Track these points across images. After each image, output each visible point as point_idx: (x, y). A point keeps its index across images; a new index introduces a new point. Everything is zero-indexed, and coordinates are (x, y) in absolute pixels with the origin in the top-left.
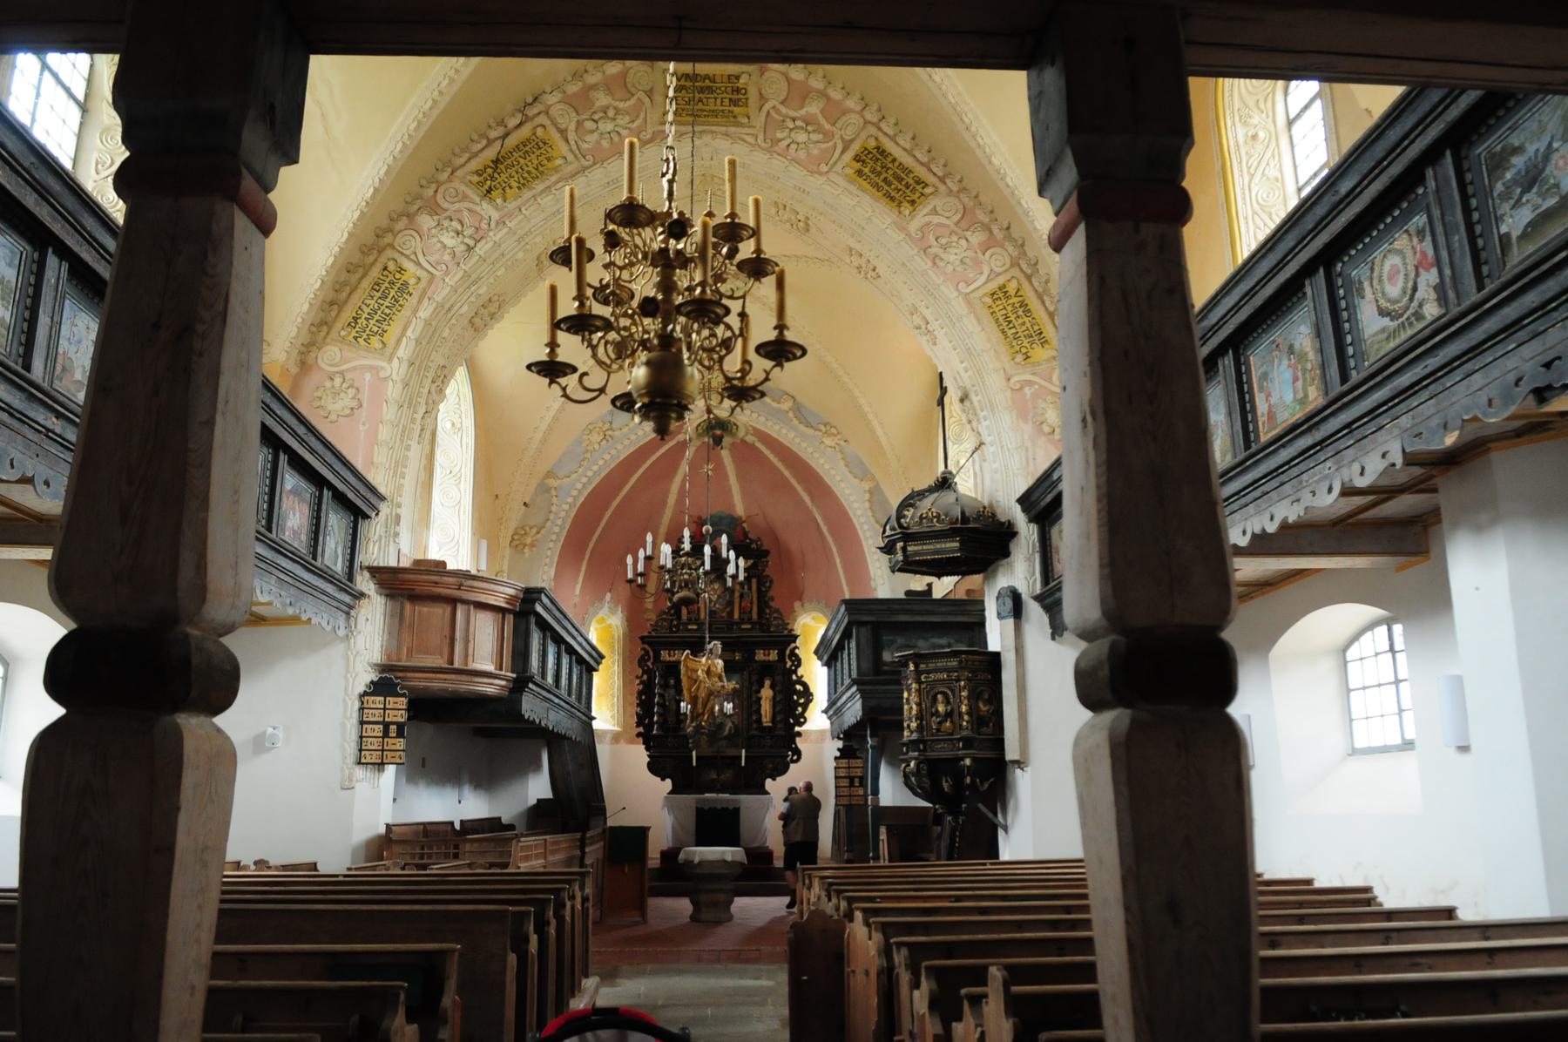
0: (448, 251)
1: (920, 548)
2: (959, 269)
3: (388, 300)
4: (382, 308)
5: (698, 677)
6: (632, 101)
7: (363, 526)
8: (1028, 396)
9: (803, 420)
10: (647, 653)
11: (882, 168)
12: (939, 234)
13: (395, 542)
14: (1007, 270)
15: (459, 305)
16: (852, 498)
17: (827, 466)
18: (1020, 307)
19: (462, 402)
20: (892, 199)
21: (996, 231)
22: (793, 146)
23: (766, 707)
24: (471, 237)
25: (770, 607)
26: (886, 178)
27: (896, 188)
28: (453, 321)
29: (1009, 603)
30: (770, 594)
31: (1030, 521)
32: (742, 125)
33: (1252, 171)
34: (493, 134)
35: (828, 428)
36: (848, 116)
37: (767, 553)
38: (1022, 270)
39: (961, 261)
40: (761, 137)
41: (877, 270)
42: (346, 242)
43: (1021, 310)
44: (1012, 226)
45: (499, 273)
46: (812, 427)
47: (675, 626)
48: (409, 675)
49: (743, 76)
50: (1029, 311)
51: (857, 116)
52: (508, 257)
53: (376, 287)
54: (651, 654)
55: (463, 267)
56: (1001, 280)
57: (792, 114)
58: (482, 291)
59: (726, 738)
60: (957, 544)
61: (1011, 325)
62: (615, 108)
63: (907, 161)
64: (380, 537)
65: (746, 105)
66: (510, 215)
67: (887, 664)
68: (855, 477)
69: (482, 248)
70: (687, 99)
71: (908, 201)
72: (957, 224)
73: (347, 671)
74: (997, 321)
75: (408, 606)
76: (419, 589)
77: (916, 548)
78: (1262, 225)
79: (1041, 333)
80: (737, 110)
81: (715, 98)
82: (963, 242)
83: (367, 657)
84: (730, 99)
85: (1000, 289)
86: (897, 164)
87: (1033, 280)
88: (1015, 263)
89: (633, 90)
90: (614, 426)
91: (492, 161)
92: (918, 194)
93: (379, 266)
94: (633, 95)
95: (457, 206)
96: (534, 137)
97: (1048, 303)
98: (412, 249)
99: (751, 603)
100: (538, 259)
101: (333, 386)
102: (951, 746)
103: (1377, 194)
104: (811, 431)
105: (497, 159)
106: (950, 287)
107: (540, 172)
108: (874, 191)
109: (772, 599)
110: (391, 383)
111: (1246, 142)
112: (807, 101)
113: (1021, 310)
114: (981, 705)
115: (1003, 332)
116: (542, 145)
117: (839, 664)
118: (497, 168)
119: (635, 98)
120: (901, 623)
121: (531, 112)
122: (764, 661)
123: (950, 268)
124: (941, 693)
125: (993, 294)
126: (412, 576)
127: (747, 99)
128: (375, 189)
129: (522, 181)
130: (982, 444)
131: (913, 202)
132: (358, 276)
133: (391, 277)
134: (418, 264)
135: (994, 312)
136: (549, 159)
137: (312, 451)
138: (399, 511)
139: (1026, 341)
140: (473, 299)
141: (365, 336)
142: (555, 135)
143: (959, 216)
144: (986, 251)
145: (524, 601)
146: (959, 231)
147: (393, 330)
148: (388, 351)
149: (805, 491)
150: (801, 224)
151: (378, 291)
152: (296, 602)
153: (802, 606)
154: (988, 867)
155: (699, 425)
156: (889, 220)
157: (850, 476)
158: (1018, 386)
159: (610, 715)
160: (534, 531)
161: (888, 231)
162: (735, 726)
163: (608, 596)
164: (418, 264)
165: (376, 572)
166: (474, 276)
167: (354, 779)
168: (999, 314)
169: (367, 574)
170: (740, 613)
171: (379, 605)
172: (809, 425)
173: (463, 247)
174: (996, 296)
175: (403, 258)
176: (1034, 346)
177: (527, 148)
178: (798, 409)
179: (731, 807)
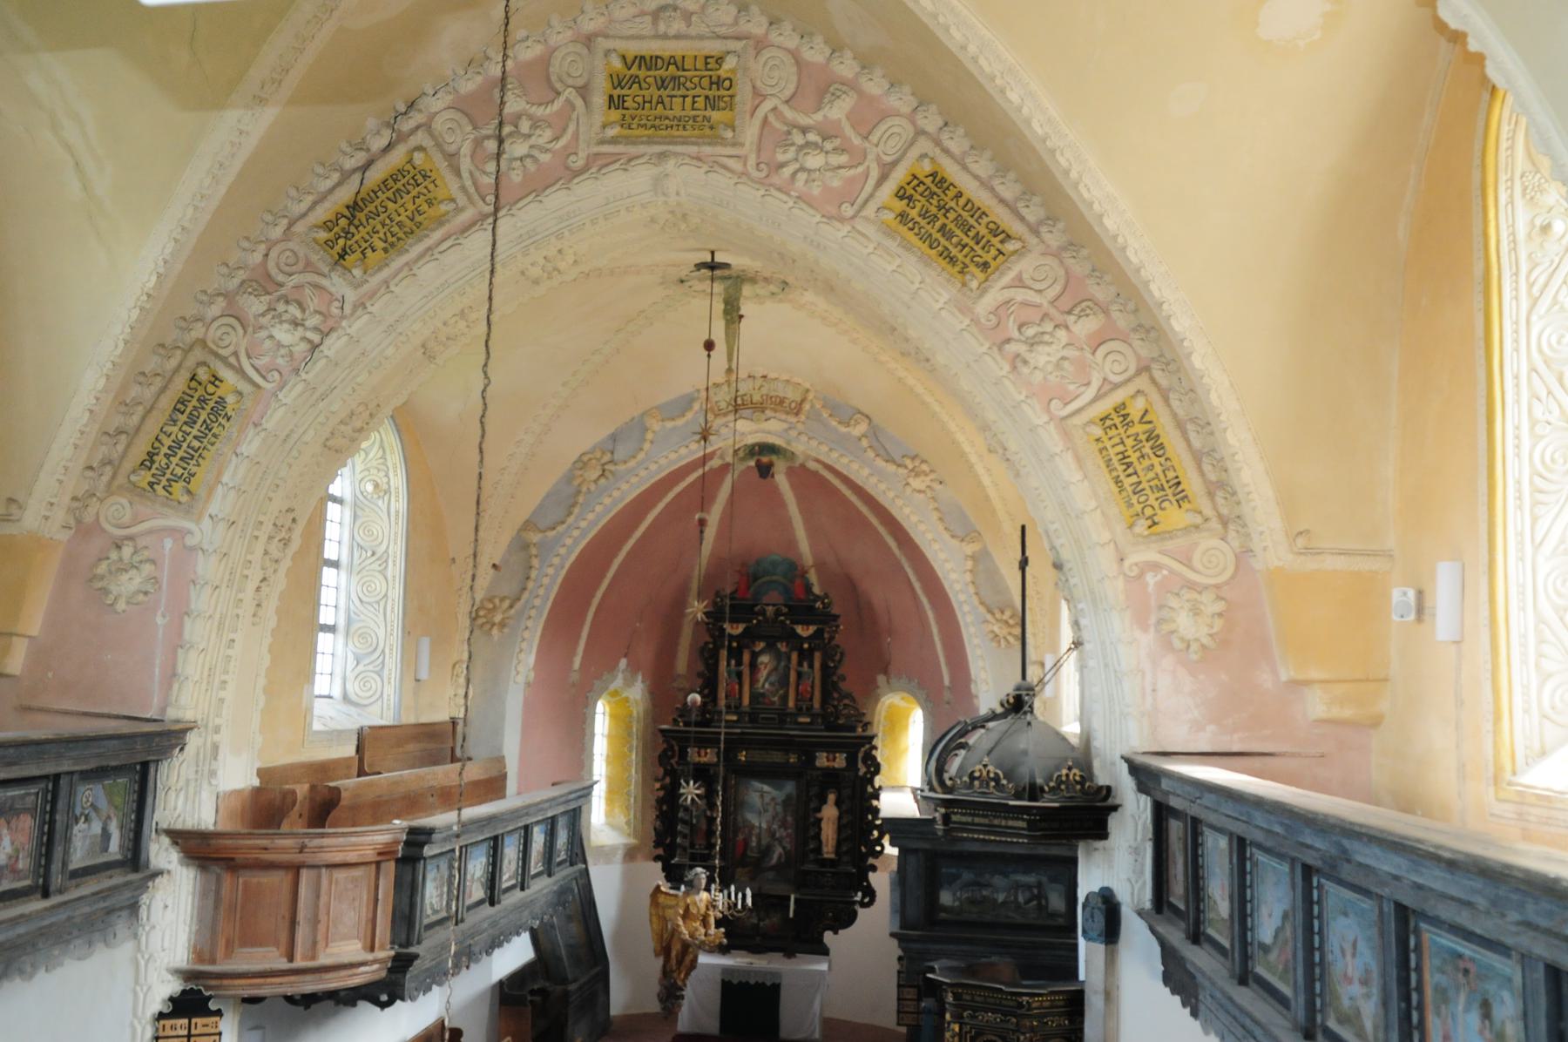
1: (969, 819)
3: (197, 426)
5: (692, 886)
6: (557, 105)
8: (1151, 589)
9: (882, 452)
10: (671, 748)
11: (940, 208)
13: (210, 783)
14: (1129, 380)
18: (1147, 440)
19: (388, 457)
20: (952, 260)
22: (802, 176)
23: (829, 833)
24: (316, 329)
26: (944, 226)
27: (959, 243)
28: (295, 453)
32: (722, 142)
33: (1536, 290)
34: (349, 164)
35: (917, 463)
36: (889, 122)
38: (1153, 381)
40: (752, 161)
42: (120, 356)
45: (359, 380)
46: (894, 462)
48: (226, 982)
49: (728, 58)
50: (1161, 446)
51: (904, 122)
53: (179, 406)
54: (676, 748)
56: (1118, 397)
57: (804, 120)
58: (334, 408)
59: (772, 868)
60: (1023, 824)
62: (530, 117)
63: (982, 198)
64: (188, 781)
65: (731, 107)
66: (372, 295)
67: (945, 909)
68: (953, 536)
69: (333, 346)
70: (639, 99)
71: (977, 265)
72: (1052, 303)
73: (137, 982)
74: (1108, 462)
75: (227, 879)
78: (1543, 394)
79: (1179, 483)
80: (715, 116)
81: (684, 97)
83: (166, 961)
84: (707, 97)
85: (1116, 410)
86: (962, 201)
89: (558, 86)
91: (348, 207)
92: (993, 252)
93: (185, 375)
94: (558, 94)
95: (296, 279)
96: (408, 167)
97: (1192, 436)
98: (231, 349)
99: (812, 687)
101: (121, 559)
104: (891, 468)
105: (355, 203)
107: (415, 227)
108: (925, 247)
109: (843, 678)
110: (200, 552)
111: (1529, 237)
112: (828, 97)
115: (1117, 481)
116: (420, 180)
118: (354, 217)
119: (562, 98)
121: (406, 125)
122: (828, 768)
126: (230, 842)
127: (731, 96)
128: (159, 276)
129: (390, 239)
131: (985, 266)
132: (154, 389)
133: (201, 391)
134: (240, 371)
135: (1105, 448)
136: (430, 203)
138: (216, 738)
139: (1152, 497)
140: (321, 419)
141: (164, 482)
142: (441, 164)
143: (1058, 288)
151: (182, 413)
156: (945, 296)
157: (946, 536)
158: (1135, 572)
159: (625, 820)
160: (507, 603)
161: (943, 313)
162: (787, 853)
163: (623, 663)
164: (240, 371)
165: (180, 837)
168: (1112, 452)
169: (166, 840)
170: (797, 700)
172: (890, 460)
173: (304, 346)
174: (1108, 423)
176: (1166, 504)
177: (399, 185)
178: (875, 433)
179: (768, 983)
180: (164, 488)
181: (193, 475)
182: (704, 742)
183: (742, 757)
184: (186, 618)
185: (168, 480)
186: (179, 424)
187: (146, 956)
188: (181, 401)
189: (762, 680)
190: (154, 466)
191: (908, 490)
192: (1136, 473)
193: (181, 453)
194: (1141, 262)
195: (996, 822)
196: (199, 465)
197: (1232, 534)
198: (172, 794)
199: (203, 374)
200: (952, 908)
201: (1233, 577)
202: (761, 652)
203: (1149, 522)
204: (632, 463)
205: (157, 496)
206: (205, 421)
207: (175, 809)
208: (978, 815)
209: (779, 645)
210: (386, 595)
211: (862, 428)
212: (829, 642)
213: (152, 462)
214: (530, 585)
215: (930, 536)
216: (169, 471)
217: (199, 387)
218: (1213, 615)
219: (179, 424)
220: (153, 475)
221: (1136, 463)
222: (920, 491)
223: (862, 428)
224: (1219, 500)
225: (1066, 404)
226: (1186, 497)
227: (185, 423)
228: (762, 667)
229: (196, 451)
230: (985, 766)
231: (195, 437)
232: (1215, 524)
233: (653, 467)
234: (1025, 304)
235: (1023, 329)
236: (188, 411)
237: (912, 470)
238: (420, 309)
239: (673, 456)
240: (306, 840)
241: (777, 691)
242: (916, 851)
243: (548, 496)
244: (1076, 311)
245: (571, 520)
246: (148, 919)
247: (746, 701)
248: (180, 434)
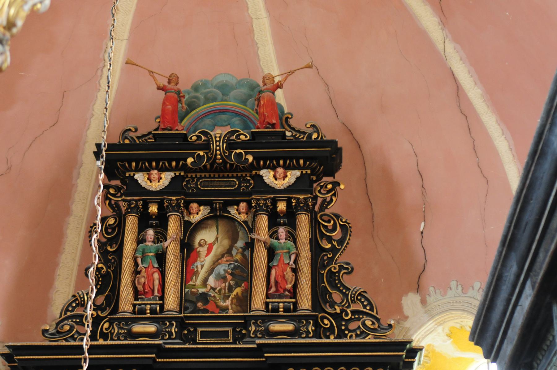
25: (344, 290)
30: (341, 258)
103: (520, 331)
117: (178, 341)
153: (424, 302)
202: (201, 225)
209: (233, 211)
212: (322, 209)
228: (203, 250)
241: (231, 289)
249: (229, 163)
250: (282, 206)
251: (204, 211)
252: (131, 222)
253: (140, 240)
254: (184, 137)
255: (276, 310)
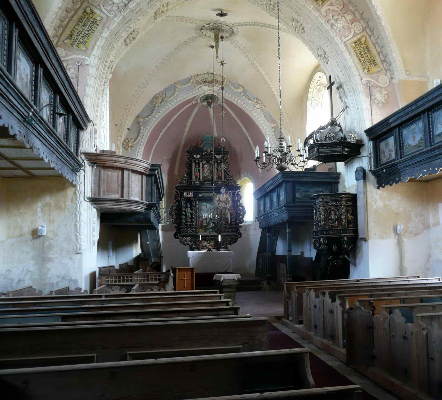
0: (116, 5)
1: (325, 150)
2: (342, 30)
3: (87, 27)
4: (84, 31)
7: (81, 133)
10: (178, 193)
12: (333, 14)
15: (121, 32)
16: (267, 130)
17: (257, 117)
18: (366, 49)
21: (357, 15)
28: (118, 39)
29: (361, 174)
31: (370, 140)
37: (188, 152)
38: (367, 33)
39: (343, 27)
41: (304, 29)
43: (366, 50)
44: (364, 13)
46: (251, 100)
47: (189, 183)
50: (370, 51)
52: (143, 10)
53: (80, 20)
54: (179, 194)
55: (123, 13)
56: (359, 37)
59: (211, 228)
61: (362, 57)
64: (88, 139)
67: (297, 198)
72: (341, 10)
74: (357, 54)
75: (102, 171)
76: (108, 164)
77: (323, 150)
79: (374, 60)
82: (343, 19)
87: (371, 37)
88: (364, 30)
90: (166, 96)
97: (377, 48)
98: (98, 3)
100: (155, 13)
102: (337, 232)
106: (338, 38)
110: (90, 66)
113: (366, 50)
114: (349, 216)
115: (359, 59)
120: (304, 182)
123: (338, 30)
124: (333, 210)
125: (355, 43)
130: (347, 107)
137: (69, 95)
141: (76, 44)
143: (342, 7)
144: (353, 23)
145: (151, 170)
146: (342, 14)
147: (91, 42)
148: (89, 52)
149: (244, 127)
150: (272, 6)
151: (81, 22)
152: (62, 168)
154: (343, 282)
155: (202, 97)
157: (267, 121)
160: (133, 140)
166: (128, 19)
167: (82, 249)
171: (89, 171)
172: (249, 99)
174: (356, 44)
175: (94, 7)
176: (371, 66)
178: (245, 91)
180: (76, 45)
181: (86, 42)
182: (188, 190)
183: (201, 195)
184: (86, 87)
185: (78, 43)
186: (80, 26)
187: (79, 192)
188: (81, 19)
189: (205, 172)
190: (72, 39)
191: (255, 108)
192: (364, 57)
193: (81, 35)
194: (338, 23)
195: (333, 149)
196: (88, 39)
197: (388, 74)
198: (84, 142)
199: (88, 10)
200: (299, 198)
201: (389, 85)
202: (205, 164)
203: (368, 70)
204: (172, 98)
205: (74, 48)
206: (89, 25)
207: (85, 147)
208: (327, 148)
209: (210, 162)
210: (104, 127)
211: (241, 90)
213: (72, 37)
214: (141, 135)
215: (262, 122)
216: (78, 41)
217: (87, 15)
218: (385, 95)
219: (80, 26)
220: (72, 42)
221: (364, 55)
222: (258, 109)
223: (241, 90)
224: (385, 65)
225: (345, 38)
226: (376, 64)
227: (83, 26)
228: (205, 168)
229: (87, 35)
230: (330, 134)
231: (86, 30)
232: (384, 71)
233: (178, 99)
234: (333, 10)
235: (334, 17)
236: (83, 22)
237: (256, 102)
238: (135, 17)
239: (184, 96)
240: (127, 160)
242: (289, 182)
243: (145, 107)
244: (347, 13)
245: (153, 114)
246: (79, 180)
247: (201, 178)
248: (81, 29)
249: (313, 387)
250: (219, 161)
251: (205, 162)
252: (194, 164)
253: (195, 167)
254: (203, 149)
255: (218, 180)
